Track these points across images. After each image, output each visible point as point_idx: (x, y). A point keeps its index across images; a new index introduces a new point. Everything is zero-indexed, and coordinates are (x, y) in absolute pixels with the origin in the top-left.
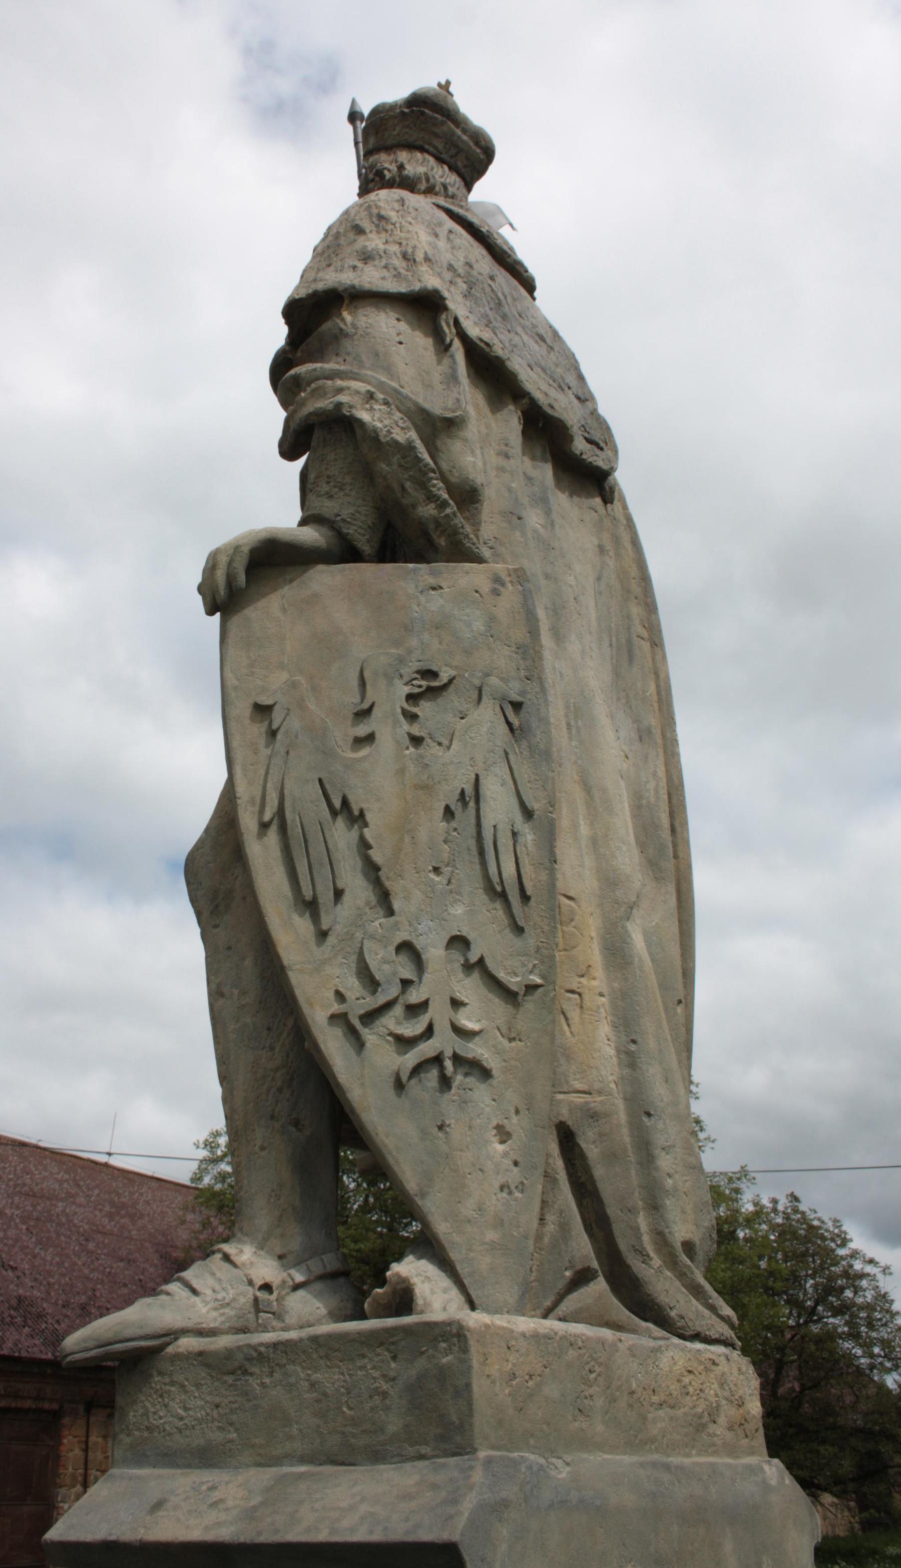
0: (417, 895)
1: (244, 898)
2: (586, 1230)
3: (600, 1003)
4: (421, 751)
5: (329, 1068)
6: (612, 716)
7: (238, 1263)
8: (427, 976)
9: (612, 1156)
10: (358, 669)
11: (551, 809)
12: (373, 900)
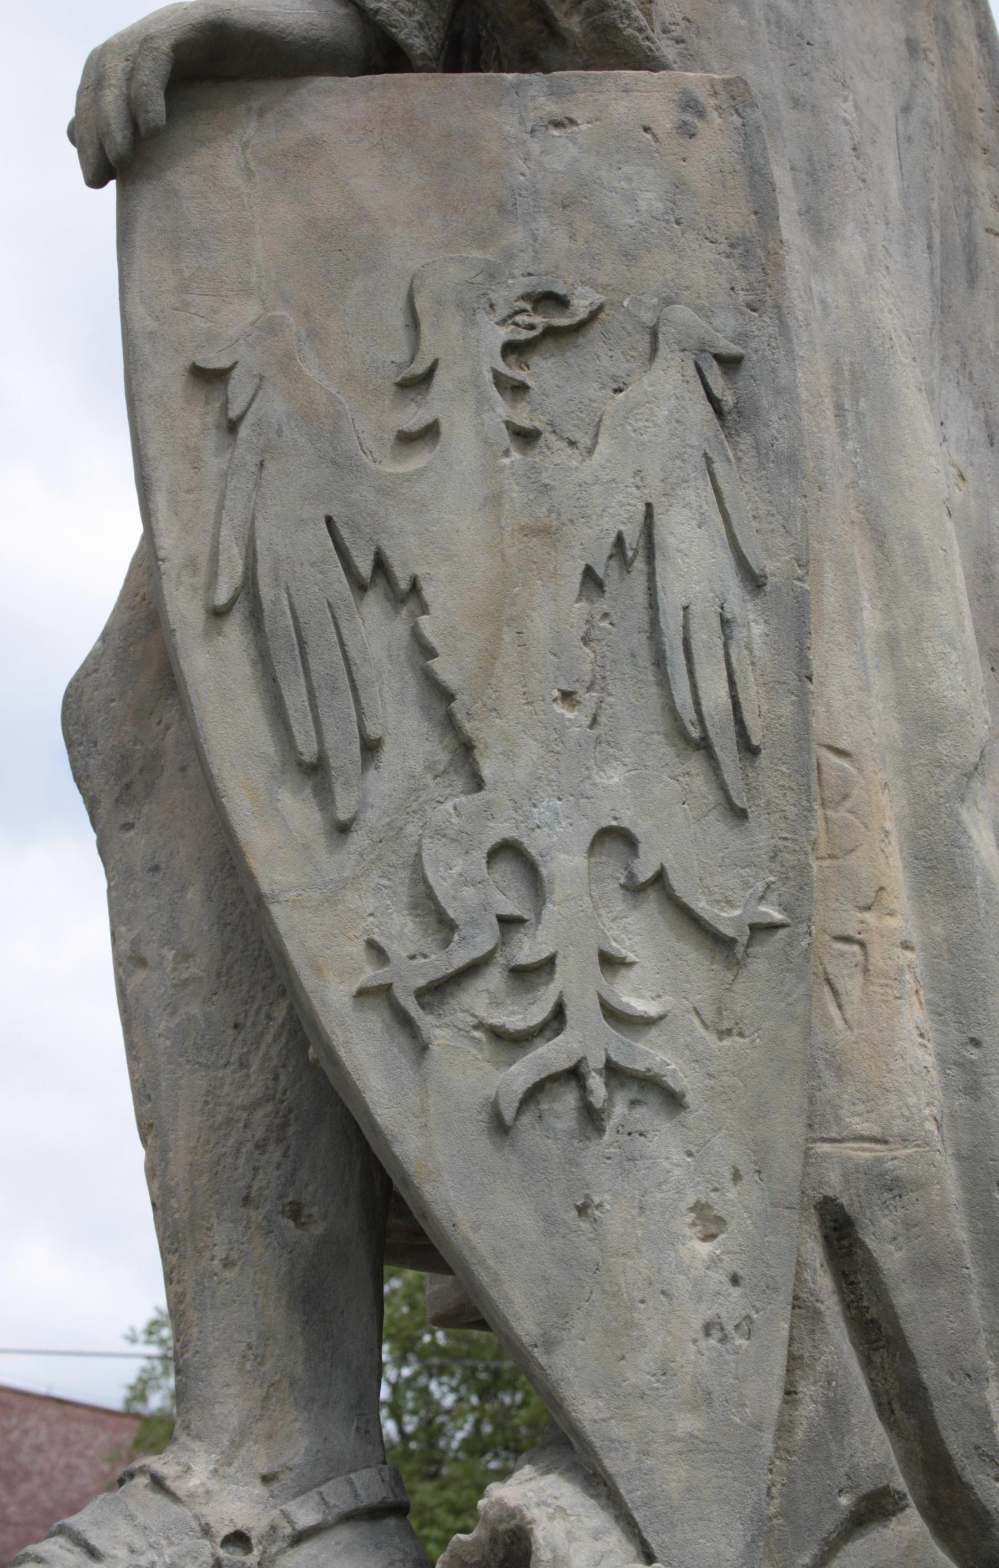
0: (530, 751)
1: (183, 769)
2: (881, 1415)
3: (903, 962)
4: (535, 457)
5: (357, 1095)
6: (930, 393)
7: (181, 1493)
8: (550, 909)
9: (931, 1268)
10: (404, 292)
11: (800, 572)
12: (443, 758)
